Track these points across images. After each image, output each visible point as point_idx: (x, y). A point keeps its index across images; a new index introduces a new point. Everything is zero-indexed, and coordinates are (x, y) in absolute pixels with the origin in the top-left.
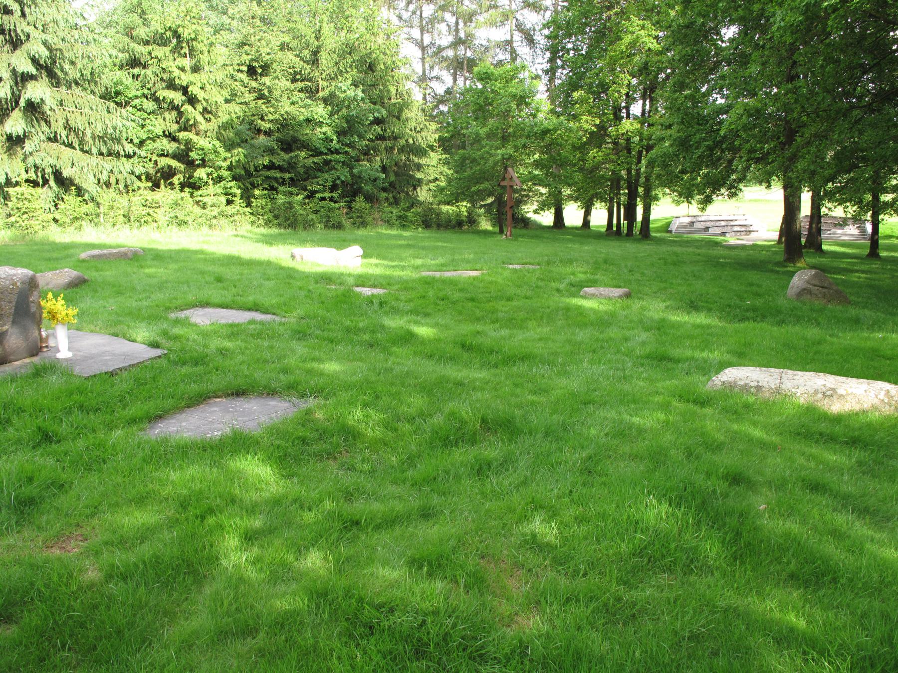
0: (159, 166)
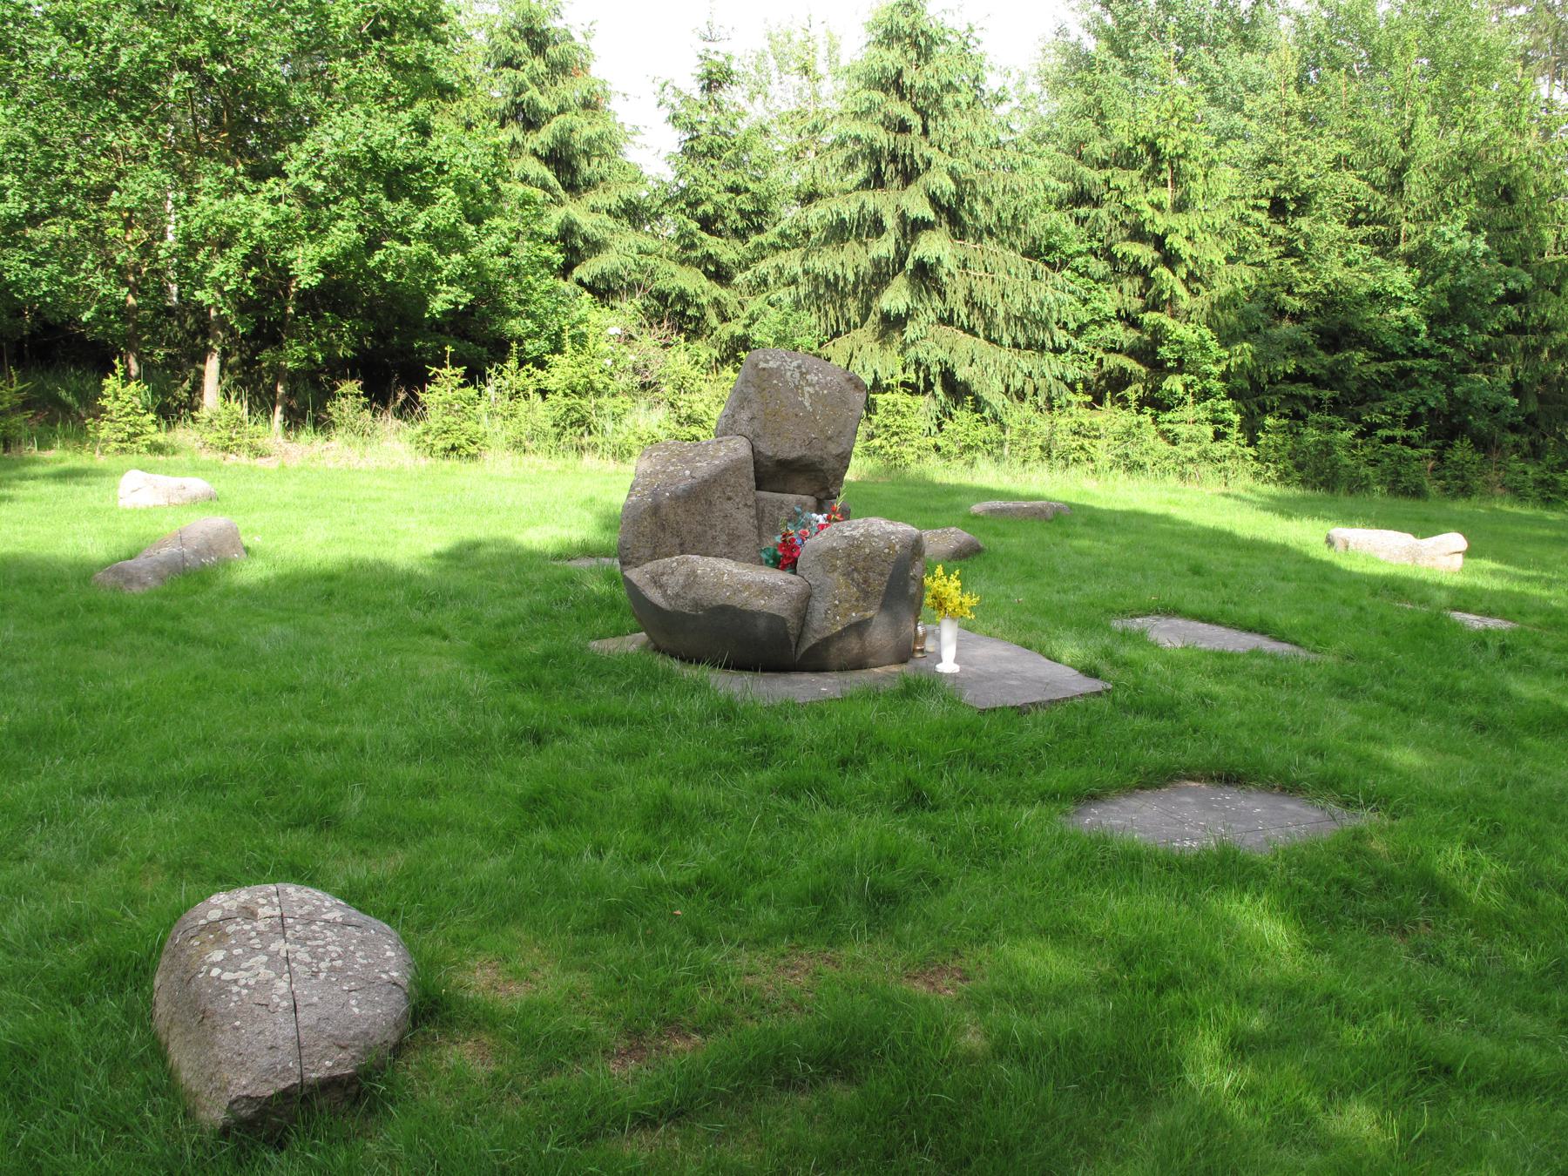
0: (1105, 369)
